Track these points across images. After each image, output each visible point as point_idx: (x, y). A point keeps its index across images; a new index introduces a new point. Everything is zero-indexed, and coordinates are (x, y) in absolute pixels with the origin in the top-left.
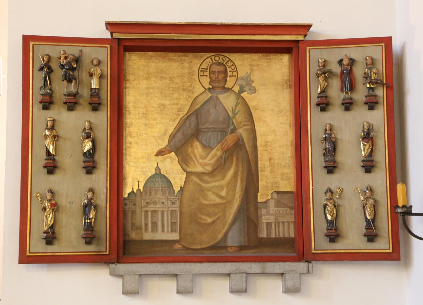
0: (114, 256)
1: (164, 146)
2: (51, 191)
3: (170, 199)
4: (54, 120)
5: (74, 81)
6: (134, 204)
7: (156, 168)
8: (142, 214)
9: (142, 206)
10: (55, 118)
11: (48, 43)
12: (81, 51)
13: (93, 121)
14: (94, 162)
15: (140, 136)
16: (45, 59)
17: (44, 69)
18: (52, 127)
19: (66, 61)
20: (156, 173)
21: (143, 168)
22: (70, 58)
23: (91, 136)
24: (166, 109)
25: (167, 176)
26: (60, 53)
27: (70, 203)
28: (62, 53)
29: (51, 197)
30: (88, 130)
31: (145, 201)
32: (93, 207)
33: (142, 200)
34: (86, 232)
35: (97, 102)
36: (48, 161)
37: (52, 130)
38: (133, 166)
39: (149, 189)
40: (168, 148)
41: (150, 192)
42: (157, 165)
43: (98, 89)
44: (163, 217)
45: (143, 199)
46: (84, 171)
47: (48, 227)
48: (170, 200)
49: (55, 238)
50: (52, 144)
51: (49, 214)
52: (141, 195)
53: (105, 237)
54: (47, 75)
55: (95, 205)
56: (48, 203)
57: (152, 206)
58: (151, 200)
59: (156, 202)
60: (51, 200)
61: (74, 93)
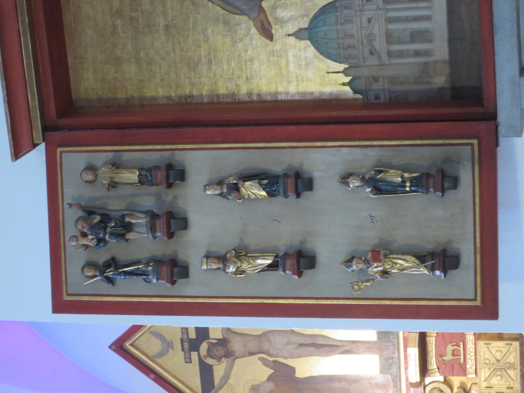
0: (481, 126)
1: (251, 23)
2: (349, 262)
3: (359, 6)
4: (207, 257)
5: (127, 219)
6: (376, 79)
7: (297, 38)
8: (394, 64)
9: (378, 63)
10: (203, 254)
11: (63, 268)
12: (70, 205)
13: (204, 179)
14: (286, 175)
15: (235, 73)
16: (90, 274)
17: (110, 276)
18: (220, 260)
19: (90, 235)
20: (308, 37)
21: (298, 65)
22: (83, 227)
23: (235, 182)
24: (175, 22)
25: (313, 15)
26: (75, 246)
27: (373, 222)
28: (74, 243)
29: (360, 261)
30: (222, 189)
31: (367, 59)
32: (380, 176)
33: (366, 64)
34: (432, 190)
35: (164, 173)
36: (287, 268)
37: (227, 260)
38: (298, 85)
39: (341, 51)
40: (254, 15)
41: (348, 49)
42: (291, 37)
43: (141, 169)
44: (398, 20)
45: (364, 62)
46: (306, 194)
47: (421, 267)
48: (363, 6)
49: (444, 251)
50: (253, 260)
51: (394, 265)
52: (355, 67)
53: (443, 148)
54: (120, 270)
55: (374, 172)
56: (373, 266)
57: (377, 44)
58: (364, 45)
59: (368, 36)
60: (366, 262)
61: (148, 219)
